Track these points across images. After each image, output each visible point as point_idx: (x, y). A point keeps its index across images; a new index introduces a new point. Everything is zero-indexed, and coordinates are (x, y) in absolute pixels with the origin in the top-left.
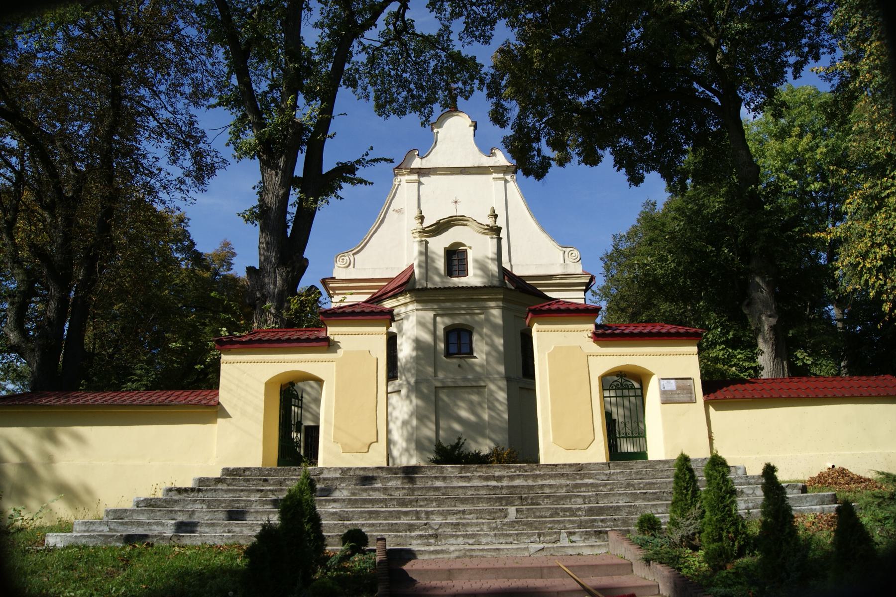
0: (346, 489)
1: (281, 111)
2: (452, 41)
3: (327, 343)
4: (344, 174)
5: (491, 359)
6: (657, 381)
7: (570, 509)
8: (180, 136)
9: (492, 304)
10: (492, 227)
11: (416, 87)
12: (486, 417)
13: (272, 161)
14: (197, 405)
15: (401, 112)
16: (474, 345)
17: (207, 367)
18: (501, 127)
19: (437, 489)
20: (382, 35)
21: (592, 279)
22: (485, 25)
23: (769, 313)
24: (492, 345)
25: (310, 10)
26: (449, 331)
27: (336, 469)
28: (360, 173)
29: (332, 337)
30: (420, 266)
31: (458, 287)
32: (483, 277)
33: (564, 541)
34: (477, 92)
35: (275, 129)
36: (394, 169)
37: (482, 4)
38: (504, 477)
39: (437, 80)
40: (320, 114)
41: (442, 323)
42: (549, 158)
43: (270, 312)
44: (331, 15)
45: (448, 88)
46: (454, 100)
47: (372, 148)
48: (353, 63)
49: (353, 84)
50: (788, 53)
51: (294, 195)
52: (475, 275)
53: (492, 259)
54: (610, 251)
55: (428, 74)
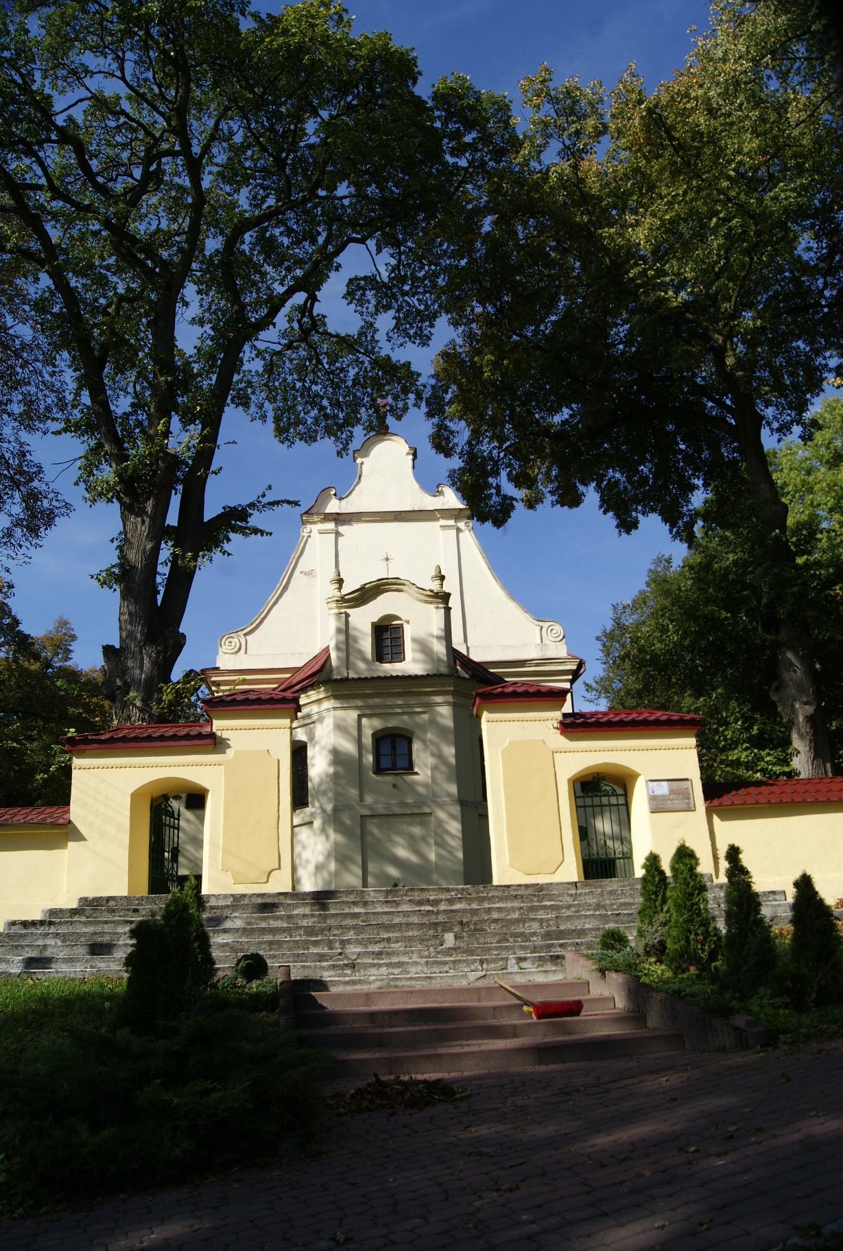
0: (240, 918)
1: (150, 439)
2: (377, 341)
3: (212, 741)
4: (233, 522)
5: (438, 776)
6: (644, 783)
7: (522, 935)
8: (6, 472)
9: (439, 699)
10: (437, 593)
11: (330, 403)
12: (432, 856)
13: (136, 505)
14: (42, 824)
15: (310, 437)
16: (414, 757)
17: (52, 778)
18: (446, 456)
19: (355, 916)
20: (284, 334)
21: (581, 664)
22: (422, 321)
23: (805, 699)
24: (440, 756)
25: (186, 304)
26: (379, 737)
27: (225, 896)
28: (255, 520)
29: (219, 734)
30: (338, 648)
31: (392, 677)
32: (425, 662)
33: (513, 966)
34: (412, 410)
35: (141, 462)
36: (302, 515)
37: (417, 293)
38: (441, 900)
39: (359, 394)
40: (200, 442)
41: (370, 726)
42: (512, 499)
43: (134, 705)
44: (214, 307)
45: (373, 405)
46: (382, 419)
47: (270, 487)
48: (244, 372)
49: (244, 401)
50: (828, 354)
51: (166, 552)
52: (414, 660)
53: (438, 638)
54: (609, 628)
55: (347, 387)
